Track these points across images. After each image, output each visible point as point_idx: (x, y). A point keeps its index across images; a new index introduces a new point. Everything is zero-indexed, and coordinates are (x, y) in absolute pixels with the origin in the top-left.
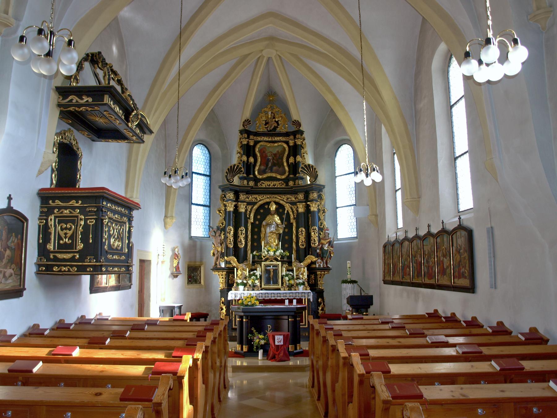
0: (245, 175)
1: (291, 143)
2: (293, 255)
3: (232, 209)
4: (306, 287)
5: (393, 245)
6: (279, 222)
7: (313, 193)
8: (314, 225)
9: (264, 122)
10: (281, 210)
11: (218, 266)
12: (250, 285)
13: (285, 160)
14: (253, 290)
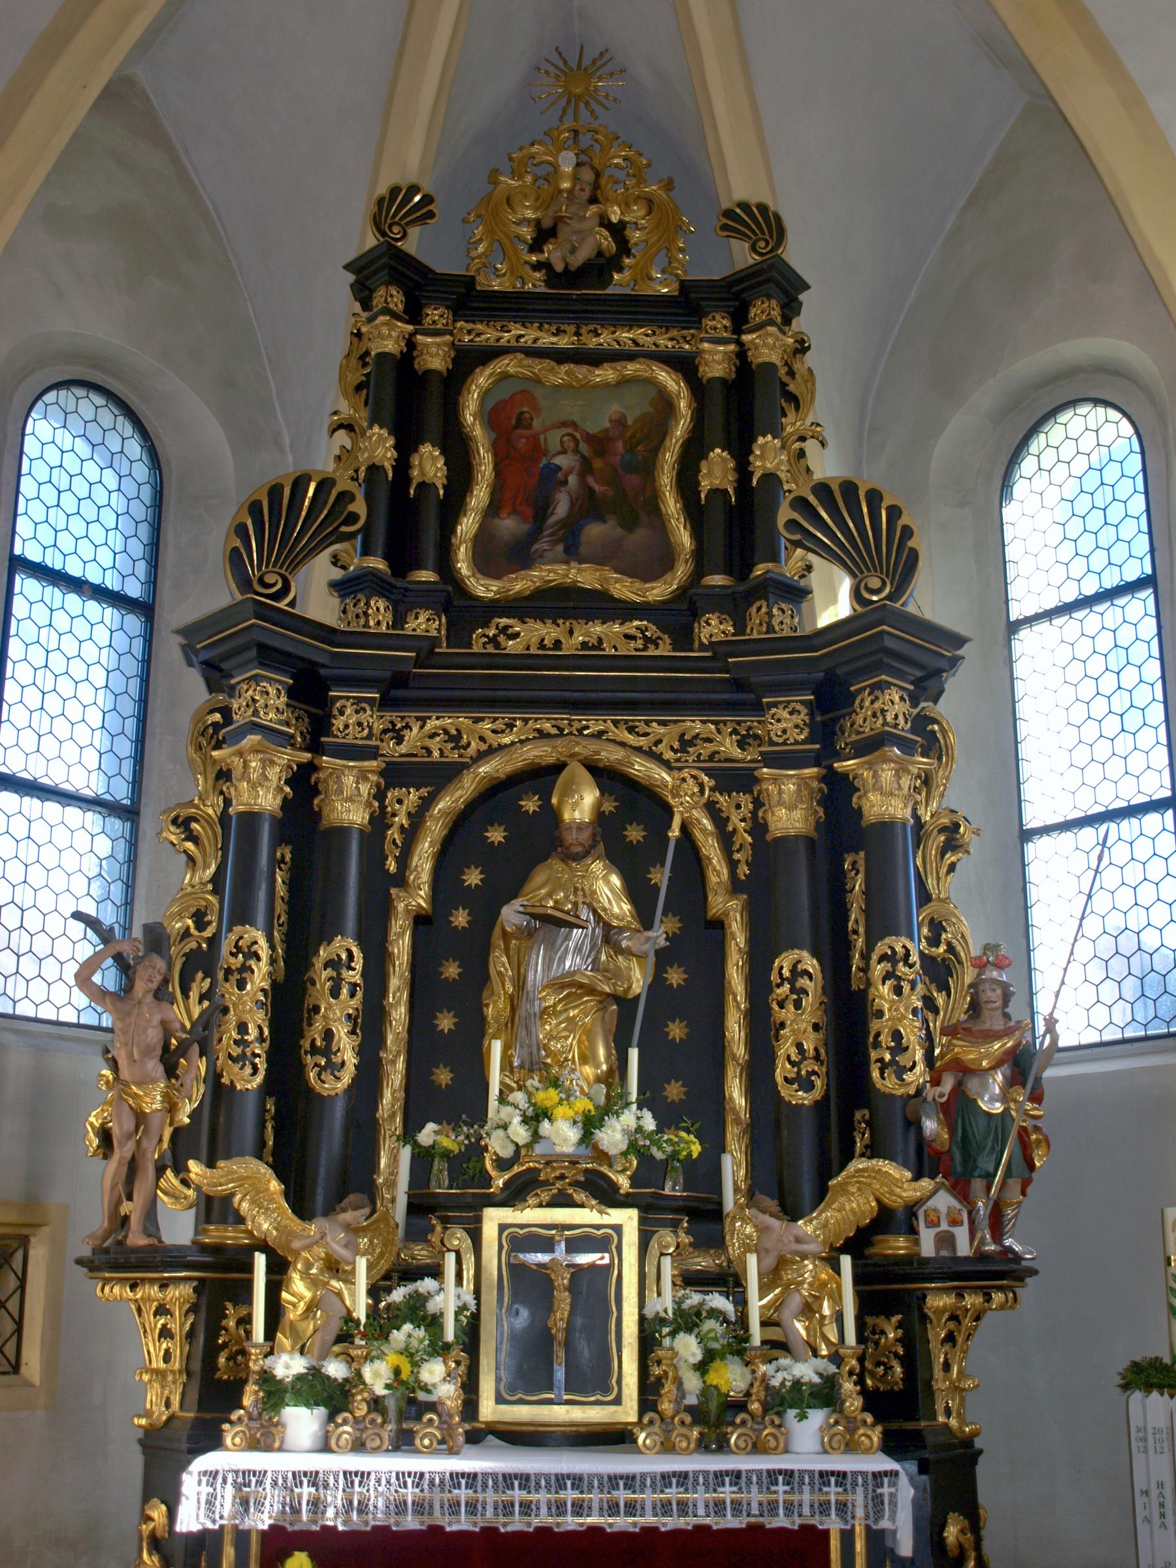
0: (378, 564)
1: (716, 362)
2: (727, 1162)
3: (268, 800)
4: (852, 1425)
5: (379, 1336)
6: (622, 909)
7: (880, 687)
8: (883, 920)
9: (527, 233)
10: (635, 834)
11: (137, 1238)
12: (376, 1404)
13: (666, 480)
14: (403, 1442)
